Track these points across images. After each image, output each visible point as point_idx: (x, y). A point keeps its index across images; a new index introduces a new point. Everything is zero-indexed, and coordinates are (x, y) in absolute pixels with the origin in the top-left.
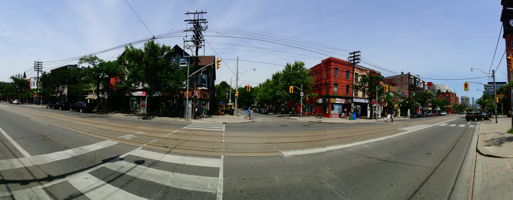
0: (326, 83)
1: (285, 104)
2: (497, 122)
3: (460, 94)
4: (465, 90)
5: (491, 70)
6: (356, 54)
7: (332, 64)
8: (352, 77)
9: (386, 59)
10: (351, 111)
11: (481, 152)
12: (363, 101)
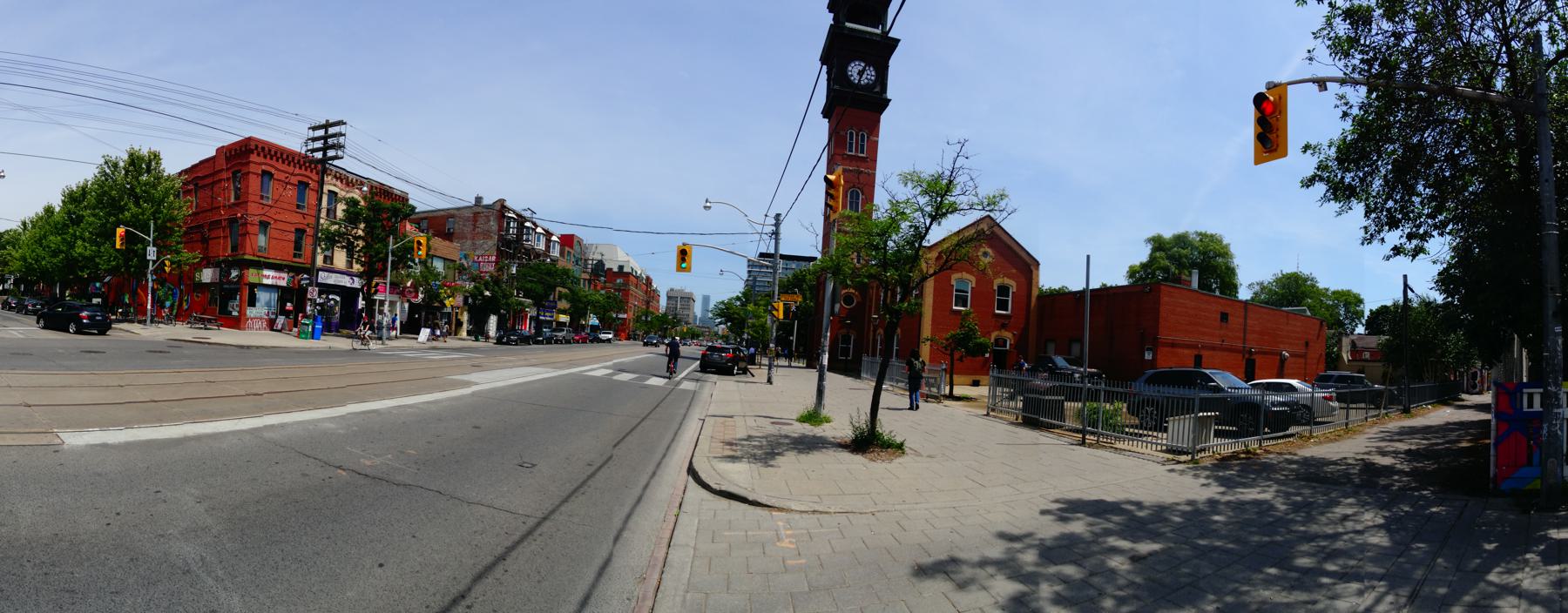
0: (233, 221)
1: (104, 284)
2: (769, 381)
3: (666, 281)
4: (680, 269)
5: (772, 214)
6: (332, 131)
7: (254, 158)
8: (313, 202)
9: (431, 155)
10: (304, 311)
11: (703, 476)
12: (345, 281)
